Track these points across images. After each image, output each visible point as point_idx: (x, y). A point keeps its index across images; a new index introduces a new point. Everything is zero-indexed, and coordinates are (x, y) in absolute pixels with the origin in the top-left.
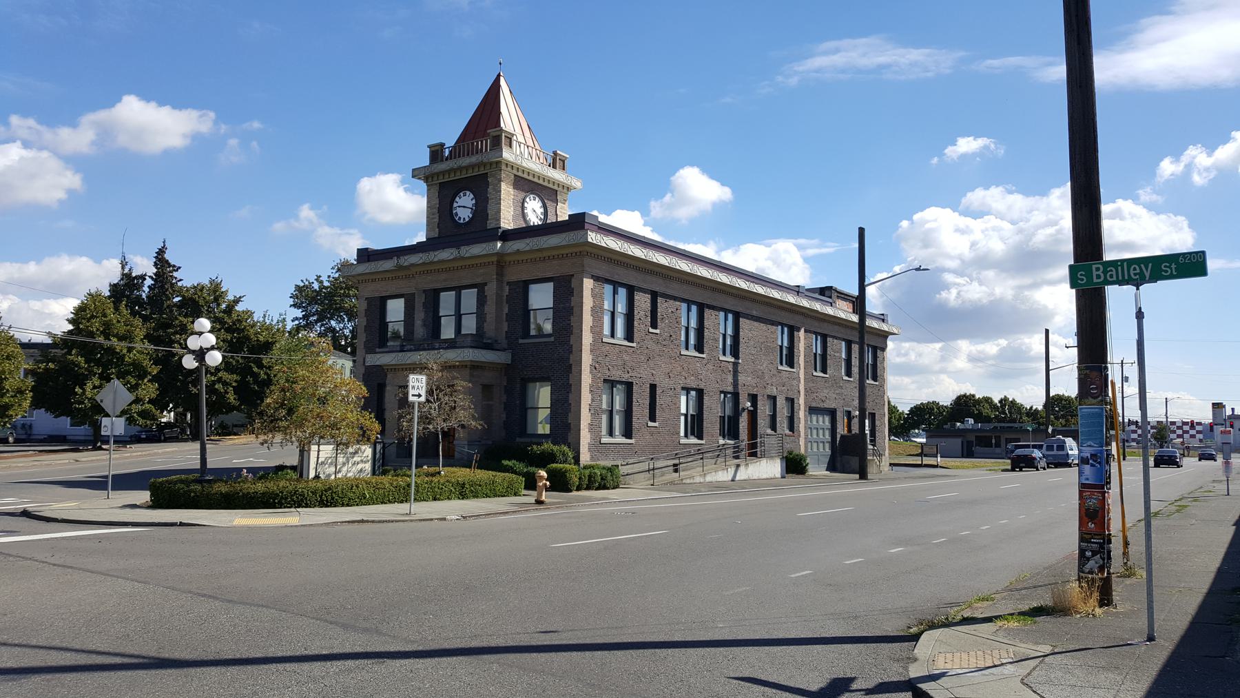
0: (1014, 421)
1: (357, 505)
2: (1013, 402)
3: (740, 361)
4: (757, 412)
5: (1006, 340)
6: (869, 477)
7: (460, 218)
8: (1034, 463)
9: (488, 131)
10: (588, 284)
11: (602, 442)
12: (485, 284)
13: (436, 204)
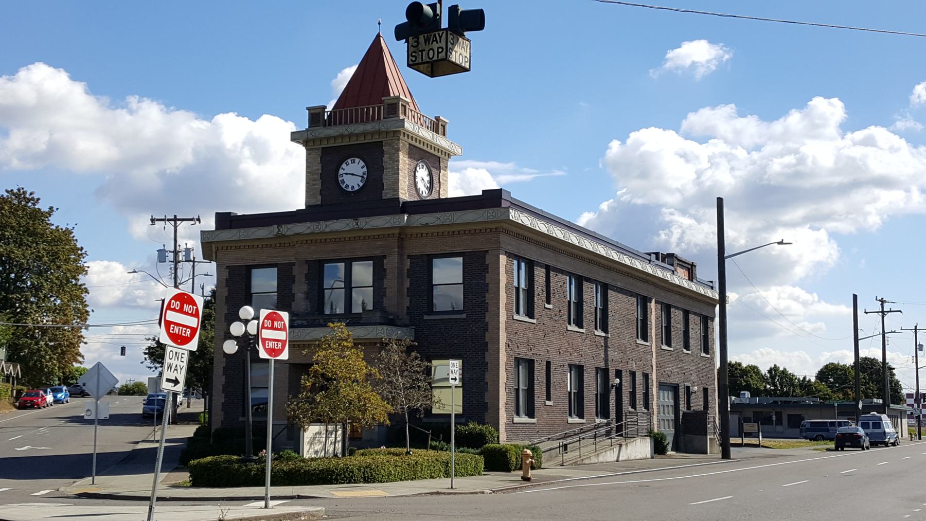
0: (786, 394)
1: (387, 482)
2: (784, 372)
3: (609, 336)
4: (622, 389)
5: (738, 293)
6: (732, 457)
7: (347, 186)
8: (860, 442)
9: (383, 99)
10: (503, 259)
11: (514, 422)
12: (385, 257)
13: (318, 170)
